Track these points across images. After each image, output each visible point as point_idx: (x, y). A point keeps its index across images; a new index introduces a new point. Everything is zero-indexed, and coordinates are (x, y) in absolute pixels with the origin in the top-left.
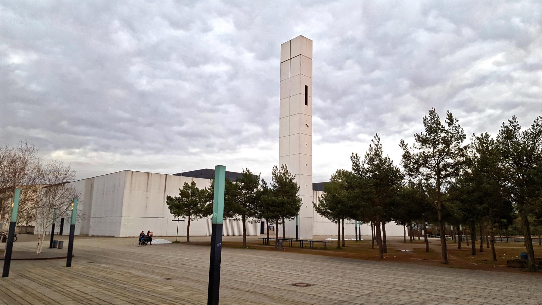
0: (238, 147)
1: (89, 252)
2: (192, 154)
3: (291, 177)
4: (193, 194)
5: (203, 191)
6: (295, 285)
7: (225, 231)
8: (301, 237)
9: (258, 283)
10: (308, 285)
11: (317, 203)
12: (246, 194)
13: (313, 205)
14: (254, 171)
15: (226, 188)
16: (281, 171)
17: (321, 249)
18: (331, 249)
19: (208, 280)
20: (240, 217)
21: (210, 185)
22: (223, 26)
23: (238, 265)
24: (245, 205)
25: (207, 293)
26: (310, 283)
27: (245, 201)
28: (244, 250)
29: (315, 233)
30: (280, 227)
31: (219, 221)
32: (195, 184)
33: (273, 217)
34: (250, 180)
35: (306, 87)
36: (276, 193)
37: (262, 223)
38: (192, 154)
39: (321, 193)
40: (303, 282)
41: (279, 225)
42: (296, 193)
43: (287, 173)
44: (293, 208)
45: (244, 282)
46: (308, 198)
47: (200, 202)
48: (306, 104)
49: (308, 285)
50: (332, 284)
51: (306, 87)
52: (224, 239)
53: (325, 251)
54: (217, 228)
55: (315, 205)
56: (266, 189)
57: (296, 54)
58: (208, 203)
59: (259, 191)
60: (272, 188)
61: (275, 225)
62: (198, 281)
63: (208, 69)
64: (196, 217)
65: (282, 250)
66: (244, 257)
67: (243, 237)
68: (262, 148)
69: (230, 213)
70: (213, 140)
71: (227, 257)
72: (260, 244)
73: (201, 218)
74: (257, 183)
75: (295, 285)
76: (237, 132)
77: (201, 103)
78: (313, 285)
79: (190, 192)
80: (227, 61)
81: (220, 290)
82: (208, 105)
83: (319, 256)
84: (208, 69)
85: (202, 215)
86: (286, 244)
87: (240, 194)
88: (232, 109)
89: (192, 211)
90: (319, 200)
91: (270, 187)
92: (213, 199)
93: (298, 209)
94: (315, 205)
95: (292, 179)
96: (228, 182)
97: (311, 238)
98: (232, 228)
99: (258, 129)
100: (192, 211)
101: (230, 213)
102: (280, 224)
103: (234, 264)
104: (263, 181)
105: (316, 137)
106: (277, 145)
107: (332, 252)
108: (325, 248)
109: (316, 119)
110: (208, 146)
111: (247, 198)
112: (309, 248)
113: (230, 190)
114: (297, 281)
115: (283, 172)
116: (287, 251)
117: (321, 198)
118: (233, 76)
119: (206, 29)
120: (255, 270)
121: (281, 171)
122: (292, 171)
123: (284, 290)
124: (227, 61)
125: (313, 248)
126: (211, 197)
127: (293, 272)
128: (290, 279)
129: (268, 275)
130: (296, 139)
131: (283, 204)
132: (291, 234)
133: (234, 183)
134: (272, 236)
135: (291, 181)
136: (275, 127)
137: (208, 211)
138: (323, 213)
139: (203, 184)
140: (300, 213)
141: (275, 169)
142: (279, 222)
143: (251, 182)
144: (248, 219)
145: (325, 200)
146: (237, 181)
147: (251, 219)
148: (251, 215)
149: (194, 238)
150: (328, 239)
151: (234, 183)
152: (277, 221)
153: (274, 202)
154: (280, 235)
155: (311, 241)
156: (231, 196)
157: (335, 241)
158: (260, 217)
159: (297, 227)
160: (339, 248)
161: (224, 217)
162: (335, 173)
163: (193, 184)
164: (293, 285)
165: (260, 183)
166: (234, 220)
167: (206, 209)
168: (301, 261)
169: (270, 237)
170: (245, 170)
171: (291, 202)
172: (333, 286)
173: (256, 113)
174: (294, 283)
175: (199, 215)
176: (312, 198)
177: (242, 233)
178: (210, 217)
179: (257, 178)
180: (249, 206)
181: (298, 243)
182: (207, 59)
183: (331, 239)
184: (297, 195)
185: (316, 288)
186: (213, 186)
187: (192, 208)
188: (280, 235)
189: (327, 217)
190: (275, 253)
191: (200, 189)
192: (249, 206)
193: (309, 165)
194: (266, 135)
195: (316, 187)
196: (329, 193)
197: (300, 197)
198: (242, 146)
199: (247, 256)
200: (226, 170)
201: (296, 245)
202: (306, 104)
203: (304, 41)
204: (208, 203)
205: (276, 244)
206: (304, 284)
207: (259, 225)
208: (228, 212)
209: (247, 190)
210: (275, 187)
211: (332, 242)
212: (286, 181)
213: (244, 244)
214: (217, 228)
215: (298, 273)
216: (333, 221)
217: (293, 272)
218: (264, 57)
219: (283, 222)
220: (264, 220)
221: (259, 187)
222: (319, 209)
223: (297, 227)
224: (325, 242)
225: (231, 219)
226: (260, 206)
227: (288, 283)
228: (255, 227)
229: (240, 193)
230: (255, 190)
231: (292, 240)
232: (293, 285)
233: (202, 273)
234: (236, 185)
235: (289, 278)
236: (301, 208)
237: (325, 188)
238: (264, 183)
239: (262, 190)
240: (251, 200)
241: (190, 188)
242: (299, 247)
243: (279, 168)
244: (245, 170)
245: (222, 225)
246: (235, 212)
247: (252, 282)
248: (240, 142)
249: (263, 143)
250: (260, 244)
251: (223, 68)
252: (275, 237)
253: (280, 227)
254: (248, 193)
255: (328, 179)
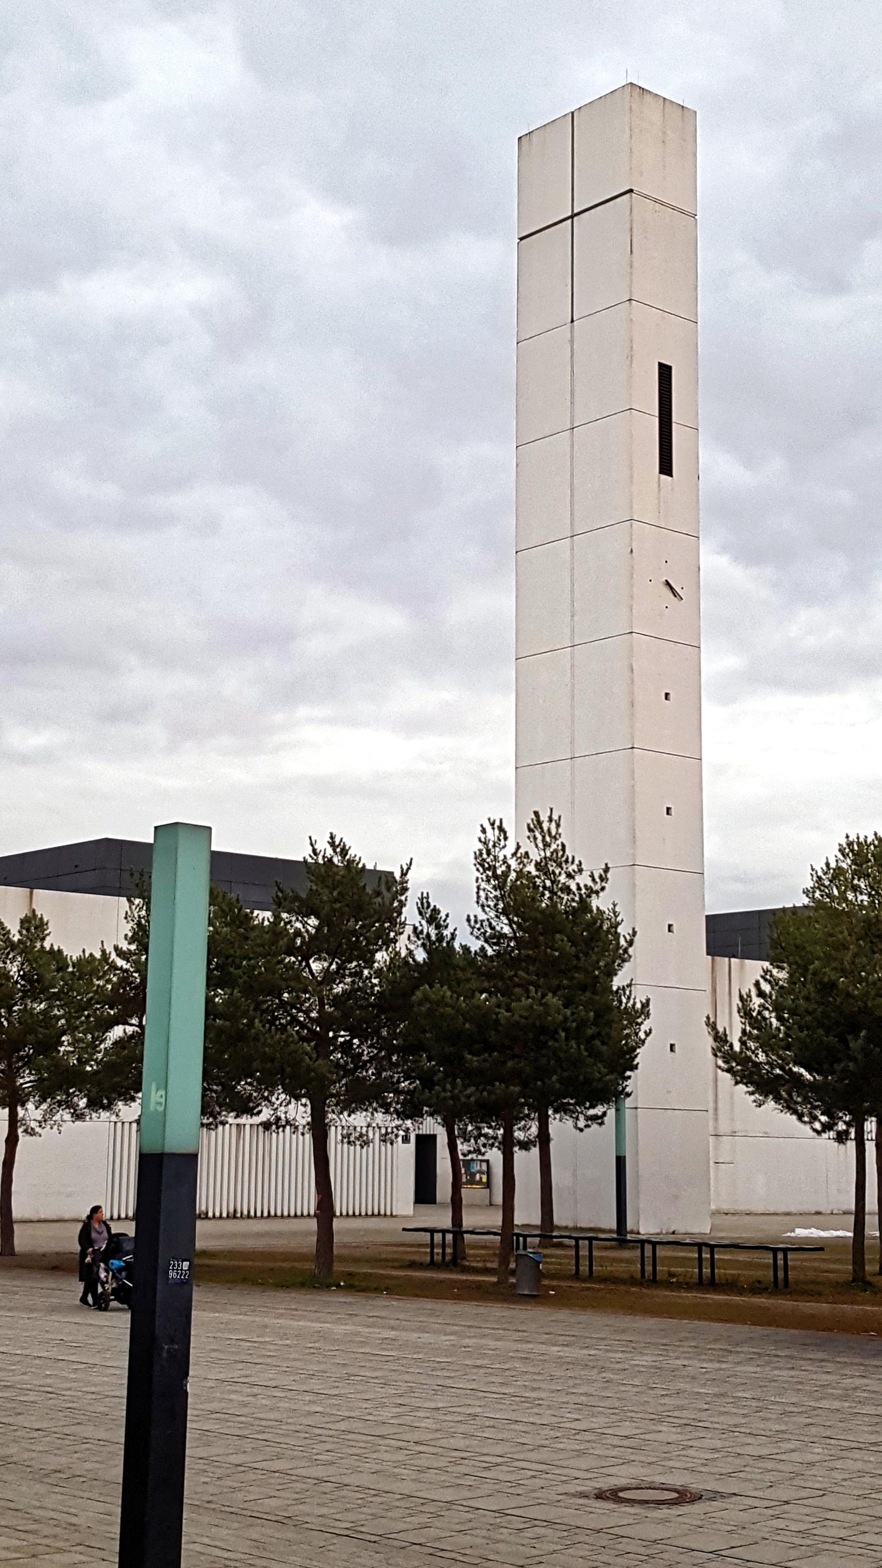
0: (279, 717)
1: (417, 1296)
2: (25, 759)
3: (583, 880)
4: (35, 986)
5: (89, 967)
6: (612, 1495)
7: (213, 1192)
8: (645, 1223)
9: (406, 1488)
10: (685, 1497)
11: (735, 1029)
12: (329, 978)
13: (710, 1042)
14: (371, 854)
15: (214, 946)
16: (527, 846)
17: (757, 1288)
18: (811, 1290)
19: (117, 1472)
20: (300, 1112)
21: (127, 928)
22: (180, 66)
23: (285, 1380)
24: (323, 1045)
25: (116, 1546)
26: (695, 1484)
27: (325, 1021)
28: (325, 1297)
29: (721, 1200)
30: (526, 1162)
31: (176, 1140)
32: (41, 926)
33: (485, 1112)
34: (347, 897)
35: (665, 372)
36: (499, 970)
37: (425, 1145)
38: (25, 759)
39: (755, 968)
40: (660, 1479)
41: (519, 1155)
42: (611, 973)
43: (559, 858)
44: (596, 1055)
45: (321, 1481)
46: (681, 998)
47: (70, 1029)
48: (666, 468)
49: (685, 1497)
50: (824, 1492)
51: (665, 372)
52: (205, 1236)
53: (784, 1304)
54: (164, 1177)
55: (720, 1039)
56: (440, 951)
57: (602, 189)
58: (118, 1032)
59: (400, 964)
60: (475, 945)
61: (495, 1156)
62: (57, 1477)
63: (107, 295)
64: (51, 1112)
65: (537, 1298)
66: (323, 1336)
67: (313, 1224)
68: (414, 725)
69: (243, 1087)
70: (138, 680)
71: (222, 1335)
72: (413, 1265)
73: (78, 1116)
74: (391, 916)
75: (612, 1495)
76: (277, 638)
77: (68, 479)
78: (716, 1495)
79: (13, 969)
80: (204, 251)
81: (186, 1528)
82: (110, 492)
83: (742, 1330)
84: (107, 295)
85: (83, 1103)
86: (557, 1259)
87: (296, 981)
88: (242, 509)
89: (26, 1079)
90: (746, 1012)
91: (467, 940)
92: (141, 1011)
93: (624, 1061)
94: (720, 1039)
95: (591, 892)
96: (227, 913)
97: (701, 1227)
98: (255, 1172)
99: (390, 620)
100: (26, 1079)
101: (243, 1087)
102: (525, 1146)
103: (266, 1377)
104: (424, 904)
105: (716, 662)
106: (505, 707)
107: (823, 1308)
108: (781, 1285)
109: (714, 562)
110: (117, 714)
111: (337, 1001)
112: (688, 1286)
113: (231, 958)
114: (621, 1476)
115: (536, 855)
116: (563, 1300)
117: (757, 1001)
118: (237, 335)
119: (93, 85)
120: (385, 1414)
121: (527, 846)
122: (586, 850)
123: (549, 1523)
124: (204, 251)
125: (711, 1284)
126: (131, 999)
127: (598, 1422)
128: (584, 1463)
129: (461, 1443)
130: (617, 670)
131: (539, 1032)
132: (584, 1205)
133: (264, 916)
134: (481, 1218)
135: (584, 905)
136: (491, 604)
137: (117, 1080)
138: (765, 1085)
139: (87, 927)
140: (636, 1082)
141: (492, 835)
142: (519, 1135)
143: (359, 909)
144: (342, 1122)
145: (778, 1009)
146: (278, 905)
147: (359, 1119)
148: (359, 1097)
149: (42, 1230)
150: (801, 1232)
151: (264, 916)
152: (509, 1133)
153: (484, 1020)
154: (527, 1213)
155: (700, 1246)
156: (249, 990)
157: (835, 1244)
158: (411, 1110)
159: (620, 1162)
160: (859, 1281)
161: (206, 1109)
162: (833, 855)
163: (34, 925)
164: (600, 1496)
165: (410, 915)
166: (267, 1126)
167: (107, 1067)
168: (644, 1360)
169: (469, 1220)
170: (323, 845)
171: (583, 1024)
172: (828, 1501)
173: (370, 527)
174: (605, 1484)
175: (69, 1105)
176: (707, 997)
177: (309, 1202)
178: (129, 1111)
179: (391, 886)
180: (346, 1048)
181: (626, 1254)
182: (94, 242)
183: (814, 1233)
184: (617, 982)
185: (731, 1513)
186: (141, 935)
187: (29, 1062)
188: (527, 1213)
189: (790, 1107)
190: (497, 1312)
191: (72, 953)
192: (346, 1048)
193: (684, 810)
194: (431, 653)
195: (729, 935)
196: (799, 969)
197: (639, 996)
198: (303, 711)
199: (340, 1329)
200: (214, 848)
201: (619, 1269)
202: (666, 468)
203: (652, 118)
204: (118, 1032)
205: (504, 1261)
206: (664, 1488)
207: (406, 1153)
208: (228, 1086)
209: (333, 955)
210: (497, 938)
211: (818, 1247)
212: (554, 905)
213: (320, 1264)
214: (164, 1177)
215: (627, 1428)
216: (826, 1127)
217: (598, 1422)
218: (403, 223)
219: (544, 1139)
220: (432, 1125)
221: (402, 945)
222: (744, 1060)
223: (620, 1162)
224: (781, 1251)
225: (245, 1120)
226: (410, 1048)
227: (572, 1488)
228: (377, 1170)
229: (298, 977)
230: (382, 957)
231: (592, 1236)
232: (600, 1496)
233: (88, 1431)
234: (276, 930)
235: (580, 1454)
236: (642, 1056)
237: (776, 944)
238: (433, 917)
239: (421, 956)
240: (354, 1012)
241: (13, 946)
242: (632, 1281)
243: (516, 835)
244: (323, 845)
245: (192, 1159)
246: (268, 1084)
247: (365, 1480)
248: (291, 692)
249: (416, 695)
250: (413, 1265)
251: (188, 291)
252: (496, 1219)
253: (526, 1162)
254: (339, 974)
255: (791, 891)
